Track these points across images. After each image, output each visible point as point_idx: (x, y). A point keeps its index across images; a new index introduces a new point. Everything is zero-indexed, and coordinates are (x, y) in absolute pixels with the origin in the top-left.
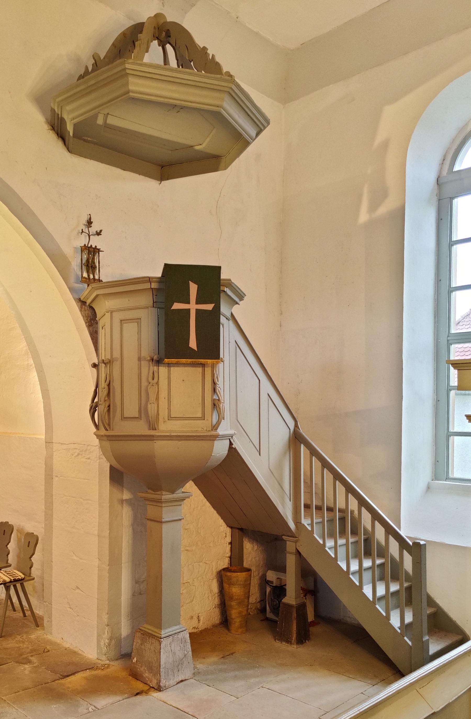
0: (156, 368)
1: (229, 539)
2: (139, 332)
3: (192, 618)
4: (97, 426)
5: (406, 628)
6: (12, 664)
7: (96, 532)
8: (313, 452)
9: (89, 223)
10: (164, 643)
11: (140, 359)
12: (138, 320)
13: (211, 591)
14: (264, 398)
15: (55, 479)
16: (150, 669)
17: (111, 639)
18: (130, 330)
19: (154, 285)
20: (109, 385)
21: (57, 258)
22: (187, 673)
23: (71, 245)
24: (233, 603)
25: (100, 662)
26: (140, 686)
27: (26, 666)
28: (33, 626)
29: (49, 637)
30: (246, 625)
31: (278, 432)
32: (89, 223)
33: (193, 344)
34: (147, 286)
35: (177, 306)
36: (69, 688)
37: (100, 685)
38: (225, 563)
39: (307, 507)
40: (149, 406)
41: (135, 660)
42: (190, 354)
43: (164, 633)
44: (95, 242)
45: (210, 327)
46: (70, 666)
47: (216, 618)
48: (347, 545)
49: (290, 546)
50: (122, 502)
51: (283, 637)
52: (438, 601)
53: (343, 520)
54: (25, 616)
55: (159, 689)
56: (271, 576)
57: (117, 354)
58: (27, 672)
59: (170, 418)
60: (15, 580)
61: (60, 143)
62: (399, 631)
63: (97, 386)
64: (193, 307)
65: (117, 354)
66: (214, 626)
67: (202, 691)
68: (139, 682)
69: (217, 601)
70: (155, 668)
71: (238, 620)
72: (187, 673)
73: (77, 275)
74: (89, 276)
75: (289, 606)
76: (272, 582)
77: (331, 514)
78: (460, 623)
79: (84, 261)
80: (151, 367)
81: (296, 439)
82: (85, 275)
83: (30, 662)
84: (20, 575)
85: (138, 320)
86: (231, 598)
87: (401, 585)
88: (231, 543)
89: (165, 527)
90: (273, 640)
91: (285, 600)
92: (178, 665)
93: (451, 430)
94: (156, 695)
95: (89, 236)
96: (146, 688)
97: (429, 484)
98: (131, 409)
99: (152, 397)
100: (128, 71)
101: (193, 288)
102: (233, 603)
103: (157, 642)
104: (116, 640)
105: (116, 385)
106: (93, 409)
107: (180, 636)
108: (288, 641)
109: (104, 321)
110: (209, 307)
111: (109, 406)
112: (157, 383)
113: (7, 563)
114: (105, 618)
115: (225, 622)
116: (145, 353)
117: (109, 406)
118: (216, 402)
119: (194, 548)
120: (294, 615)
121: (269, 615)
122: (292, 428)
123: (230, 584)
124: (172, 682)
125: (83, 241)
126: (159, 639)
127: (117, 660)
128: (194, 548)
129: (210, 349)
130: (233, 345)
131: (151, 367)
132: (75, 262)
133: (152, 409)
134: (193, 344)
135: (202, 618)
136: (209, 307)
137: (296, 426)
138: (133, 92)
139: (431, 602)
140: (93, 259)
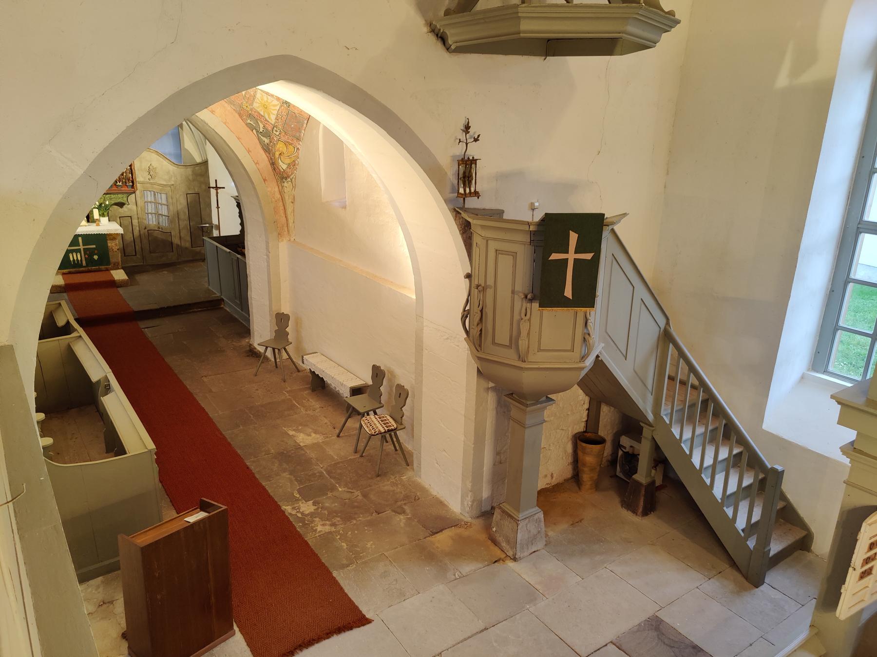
0: (529, 305)
1: (586, 406)
2: (515, 266)
3: (546, 476)
4: (467, 332)
5: (751, 528)
6: (389, 512)
7: (463, 412)
8: (682, 354)
9: (467, 128)
10: (522, 524)
11: (513, 292)
12: (514, 255)
13: (565, 451)
14: (637, 302)
15: (425, 352)
16: (508, 542)
17: (473, 502)
18: (505, 262)
19: (532, 228)
20: (481, 311)
21: (432, 171)
22: (540, 545)
23: (446, 154)
24: (586, 469)
25: (463, 517)
26: (498, 553)
27: (402, 517)
28: (404, 463)
29: (419, 480)
30: (597, 486)
31: (647, 332)
32: (467, 128)
33: (568, 293)
34: (526, 228)
35: (555, 256)
36: (437, 547)
37: (463, 549)
38: (580, 428)
39: (671, 378)
40: (520, 342)
41: (494, 529)
42: (565, 303)
43: (521, 516)
44: (474, 151)
45: (587, 275)
46: (437, 521)
47: (568, 473)
48: (705, 434)
49: (646, 432)
50: (488, 389)
51: (629, 505)
52: (789, 496)
53: (705, 403)
54: (396, 450)
55: (515, 559)
56: (625, 441)
57: (490, 282)
58: (402, 524)
59: (539, 350)
60: (389, 431)
61: (439, 44)
62: (742, 534)
63: (469, 295)
64: (571, 256)
65: (490, 282)
66: (566, 480)
67: (552, 566)
68: (496, 549)
69: (570, 459)
70: (513, 544)
71: (589, 483)
72: (540, 545)
73: (453, 185)
74: (465, 191)
75: (638, 484)
76: (625, 448)
77: (695, 393)
78: (807, 520)
79: (461, 175)
80: (524, 304)
81: (666, 337)
82: (461, 191)
83: (403, 512)
84: (393, 425)
85: (514, 255)
86: (584, 465)
87: (756, 477)
88: (588, 409)
89: (527, 431)
90: (619, 506)
91: (636, 477)
92: (532, 540)
93: (852, 276)
94: (510, 564)
95: (467, 144)
96: (503, 556)
97: (803, 374)
98: (503, 336)
99: (524, 333)
100: (520, 15)
101: (573, 237)
102: (586, 469)
103: (515, 524)
104: (478, 501)
105: (489, 311)
106: (465, 315)
107: (536, 517)
108: (634, 512)
109: (476, 239)
110: (588, 256)
111: (481, 330)
112: (529, 320)
113: (380, 403)
114: (469, 485)
115: (576, 477)
116: (519, 287)
117: (481, 330)
118: (587, 336)
119: (552, 418)
120: (643, 492)
121: (619, 473)
122: (662, 327)
123: (584, 453)
124: (526, 554)
125: (459, 150)
126: (516, 521)
127: (478, 517)
128: (552, 418)
129: (585, 296)
130: (610, 257)
131: (524, 304)
132: (451, 171)
133: (523, 344)
134: (568, 293)
135: (555, 475)
136: (588, 256)
137: (668, 323)
138: (525, 32)
139: (783, 497)
140: (470, 171)
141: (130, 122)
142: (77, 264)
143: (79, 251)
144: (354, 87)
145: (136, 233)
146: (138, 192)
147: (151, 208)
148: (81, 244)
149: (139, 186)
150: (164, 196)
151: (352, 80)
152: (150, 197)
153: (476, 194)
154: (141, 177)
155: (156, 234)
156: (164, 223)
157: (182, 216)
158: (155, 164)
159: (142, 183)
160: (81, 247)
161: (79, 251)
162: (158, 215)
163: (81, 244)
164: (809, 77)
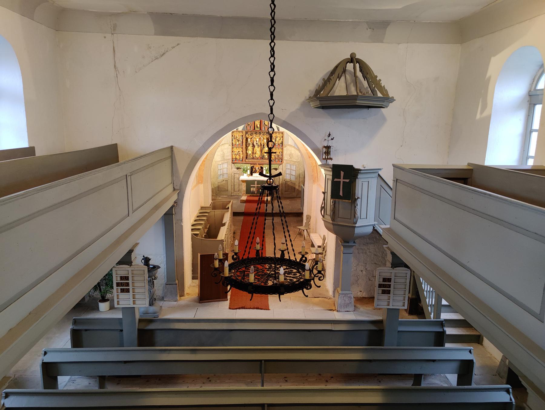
9: (330, 135)
32: (330, 135)
33: (341, 194)
134: (341, 194)
141: (215, 132)
142: (253, 192)
143: (254, 187)
144: (284, 121)
145: (281, 182)
146: (284, 164)
147: (288, 171)
148: (339, 180)
149: (284, 161)
150: (294, 167)
151: (284, 119)
152: (288, 167)
153: (331, 159)
154: (286, 157)
155: (289, 183)
156: (293, 179)
157: (301, 176)
158: (293, 152)
159: (286, 160)
160: (256, 186)
161: (254, 187)
162: (291, 175)
163: (339, 180)
164: (485, 114)
